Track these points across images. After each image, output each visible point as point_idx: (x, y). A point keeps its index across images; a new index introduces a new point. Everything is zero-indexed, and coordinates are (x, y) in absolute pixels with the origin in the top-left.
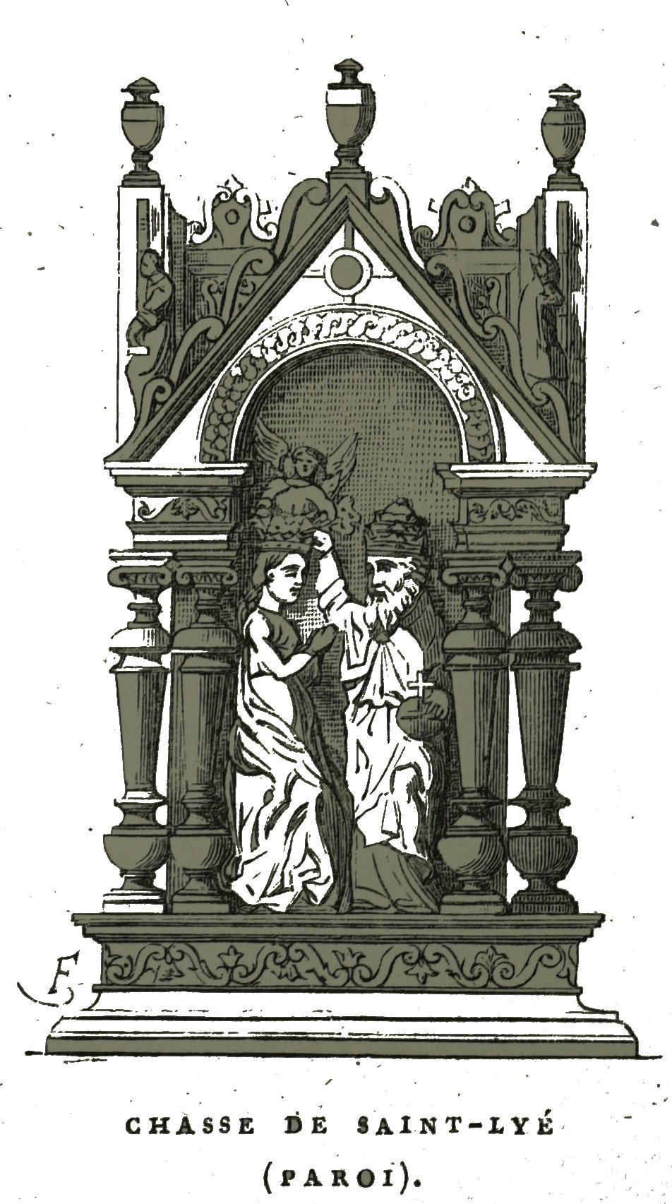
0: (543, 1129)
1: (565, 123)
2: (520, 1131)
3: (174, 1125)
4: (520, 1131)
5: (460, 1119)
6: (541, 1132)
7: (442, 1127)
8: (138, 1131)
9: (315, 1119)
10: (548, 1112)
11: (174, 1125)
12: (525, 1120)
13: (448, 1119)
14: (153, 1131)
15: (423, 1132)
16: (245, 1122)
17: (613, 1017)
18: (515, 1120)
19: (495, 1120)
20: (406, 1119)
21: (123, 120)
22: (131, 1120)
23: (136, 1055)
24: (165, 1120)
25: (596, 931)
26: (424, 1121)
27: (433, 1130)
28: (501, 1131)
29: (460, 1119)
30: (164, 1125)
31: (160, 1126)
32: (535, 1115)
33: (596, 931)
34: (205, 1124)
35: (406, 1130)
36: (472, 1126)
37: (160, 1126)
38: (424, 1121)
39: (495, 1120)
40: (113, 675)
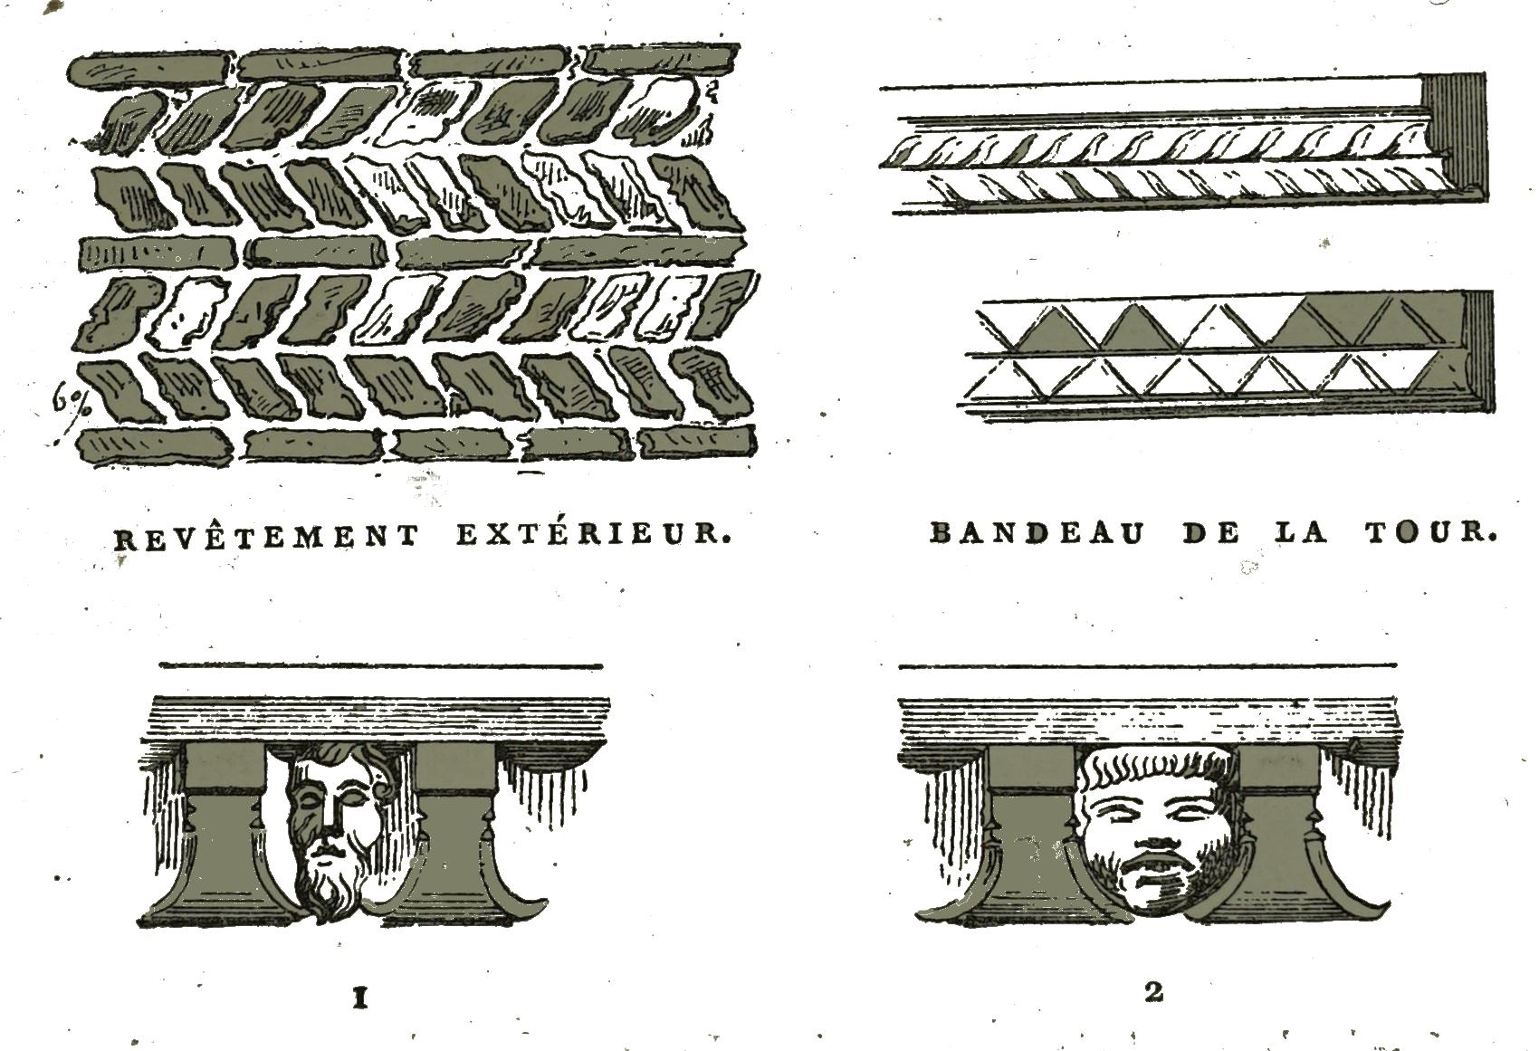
0: (1375, 527)
3: (328, 537)
6: (636, 540)
10: (561, 516)
13: (237, 532)
15: (998, 540)
17: (117, 388)
20: (615, 526)
25: (636, 45)
26: (371, 529)
27: (382, 542)
29: (415, 528)
33: (636, 45)
35: (615, 540)
38: (371, 529)
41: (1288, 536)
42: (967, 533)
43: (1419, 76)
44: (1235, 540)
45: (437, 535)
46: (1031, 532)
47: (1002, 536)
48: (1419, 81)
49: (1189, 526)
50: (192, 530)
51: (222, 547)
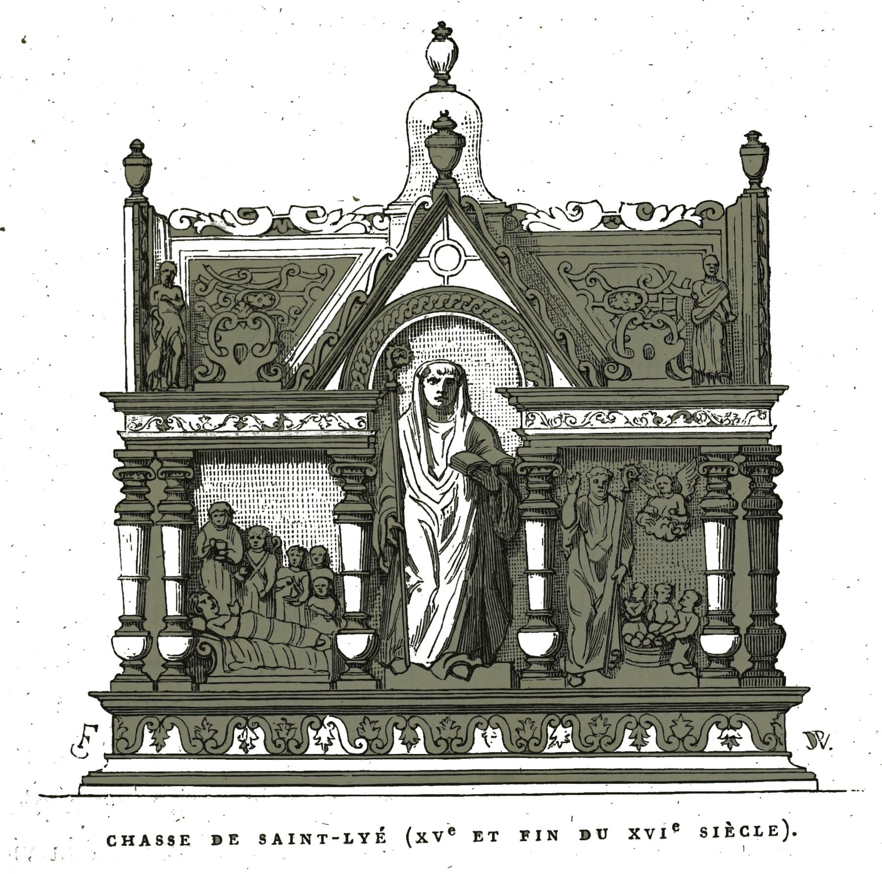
0: (477, 834)
1: (755, 152)
2: (364, 842)
3: (138, 840)
4: (364, 842)
5: (497, 833)
7: (315, 840)
8: (748, 835)
9: (182, 836)
11: (138, 840)
12: (367, 834)
14: (124, 844)
16: (233, 837)
18: (361, 834)
19: (347, 835)
20: (292, 835)
21: (741, 156)
22: (110, 836)
23: (746, 781)
24: (132, 837)
26: (550, 832)
27: (309, 842)
28: (352, 842)
29: (497, 833)
30: (131, 840)
31: (128, 840)
32: (374, 830)
34: (158, 840)
35: (291, 843)
36: (334, 838)
37: (128, 840)
38: (303, 836)
39: (347, 835)
40: (746, 521)
41: (349, 840)
42: (275, 840)
43: (756, 195)
44: (777, 834)
45: (201, 840)
46: (214, 839)
47: (305, 841)
48: (729, 186)
49: (214, 837)
50: (653, 830)
51: (777, 834)
